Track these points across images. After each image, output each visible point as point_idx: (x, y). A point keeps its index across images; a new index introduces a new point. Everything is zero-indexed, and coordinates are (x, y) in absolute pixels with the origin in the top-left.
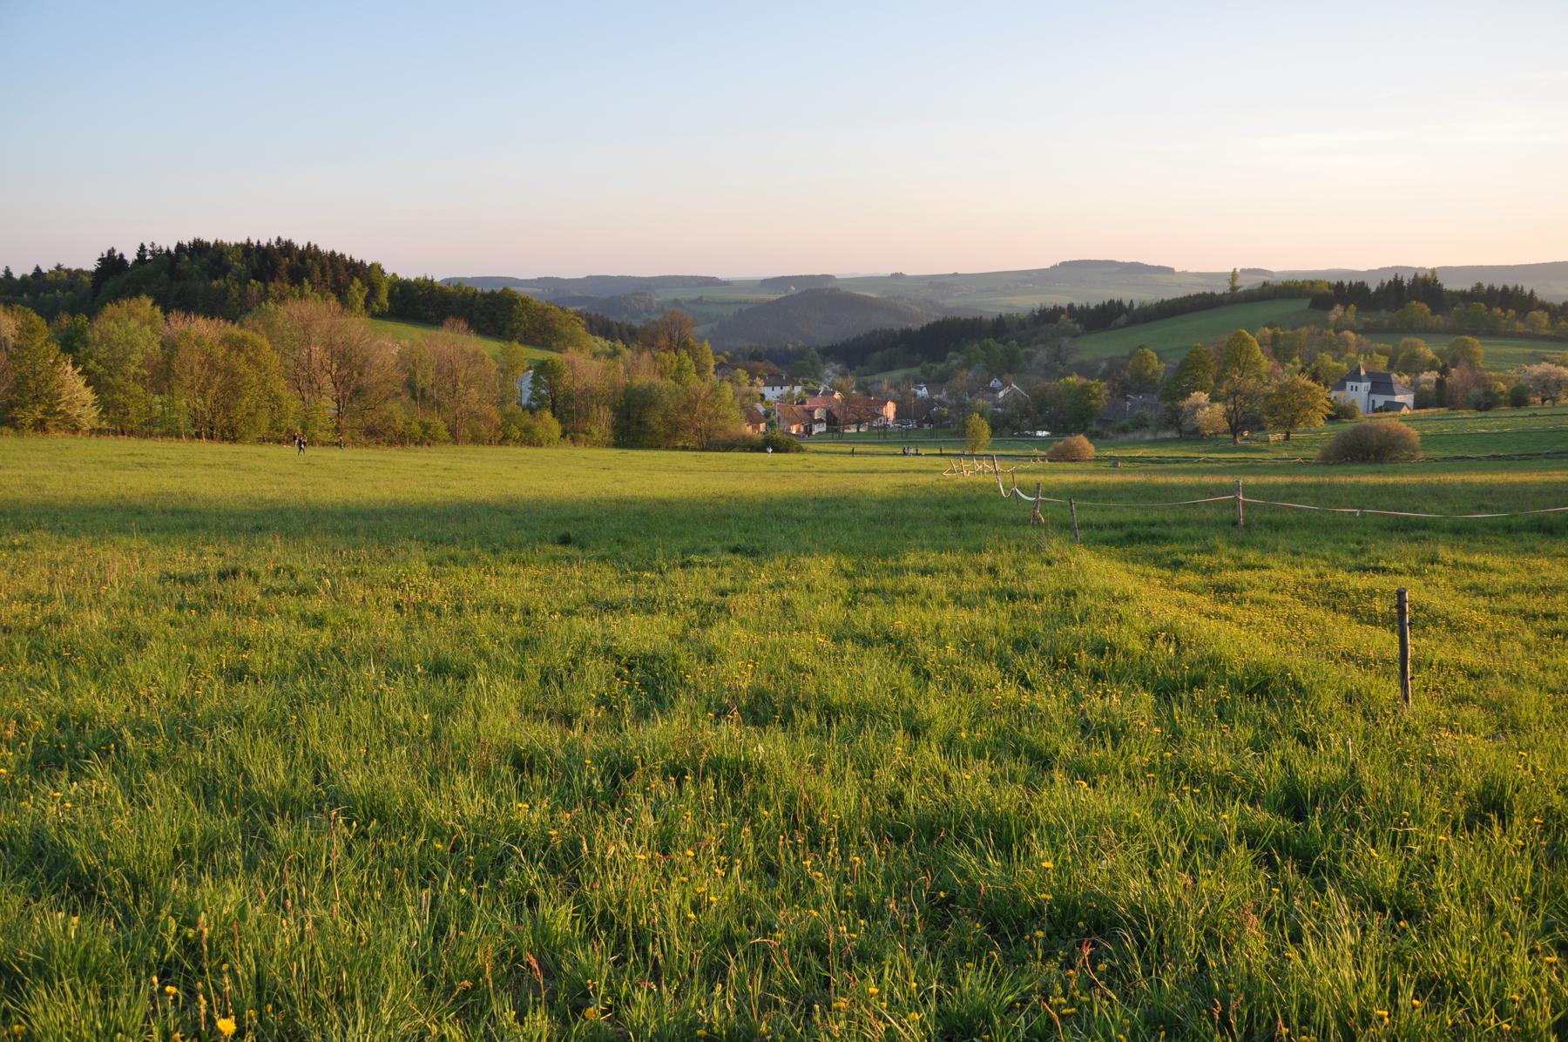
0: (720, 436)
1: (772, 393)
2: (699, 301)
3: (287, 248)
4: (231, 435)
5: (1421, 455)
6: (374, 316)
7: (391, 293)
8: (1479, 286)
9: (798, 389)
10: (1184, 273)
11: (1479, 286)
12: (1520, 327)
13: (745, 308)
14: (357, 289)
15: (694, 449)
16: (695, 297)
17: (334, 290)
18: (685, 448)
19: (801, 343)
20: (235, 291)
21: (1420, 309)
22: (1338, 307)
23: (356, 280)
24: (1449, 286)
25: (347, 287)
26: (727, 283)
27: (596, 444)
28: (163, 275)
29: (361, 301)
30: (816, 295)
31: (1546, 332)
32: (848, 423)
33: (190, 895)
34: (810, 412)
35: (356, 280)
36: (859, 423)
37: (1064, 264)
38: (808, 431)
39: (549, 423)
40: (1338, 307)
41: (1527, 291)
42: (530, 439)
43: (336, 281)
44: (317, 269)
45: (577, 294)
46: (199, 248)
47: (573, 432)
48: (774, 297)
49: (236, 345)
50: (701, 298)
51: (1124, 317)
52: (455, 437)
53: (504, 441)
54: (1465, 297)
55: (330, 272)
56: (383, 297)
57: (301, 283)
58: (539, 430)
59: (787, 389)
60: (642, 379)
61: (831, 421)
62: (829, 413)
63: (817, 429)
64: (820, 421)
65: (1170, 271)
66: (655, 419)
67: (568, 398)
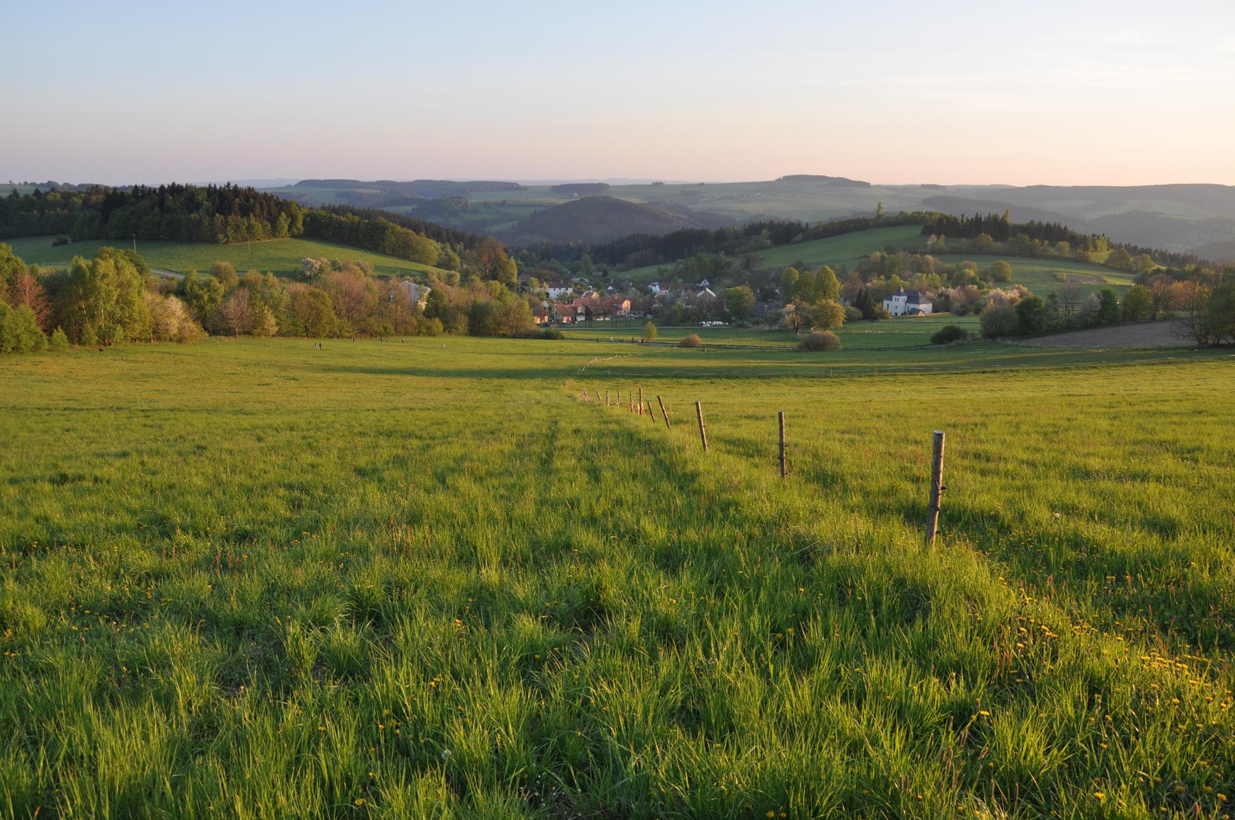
0: (523, 330)
1: (554, 293)
2: (503, 204)
3: (236, 191)
4: (315, 336)
5: (841, 347)
6: (294, 236)
7: (304, 221)
8: (1032, 222)
9: (570, 290)
10: (879, 186)
11: (1032, 222)
12: (1052, 251)
13: (538, 210)
14: (283, 221)
15: (509, 337)
16: (499, 200)
17: (268, 220)
18: (504, 336)
19: (580, 241)
20: (206, 220)
21: (986, 239)
22: (933, 236)
23: (283, 214)
24: (1012, 220)
25: (277, 218)
26: (525, 188)
27: (460, 334)
28: (157, 209)
29: (286, 227)
30: (593, 201)
31: (1067, 255)
32: (598, 315)
33: (37, 682)
34: (575, 309)
35: (283, 214)
36: (605, 315)
37: (786, 178)
38: (574, 319)
39: (438, 324)
40: (933, 236)
41: (1062, 226)
42: (430, 333)
43: (270, 213)
44: (258, 205)
45: (408, 195)
46: (175, 190)
47: (449, 329)
48: (562, 202)
49: (316, 296)
50: (504, 202)
51: (800, 236)
52: (397, 332)
53: (418, 334)
54: (1025, 229)
55: (266, 209)
56: (300, 224)
57: (248, 216)
58: (435, 329)
59: (563, 290)
60: (482, 299)
61: (588, 314)
62: (587, 309)
63: (580, 319)
64: (581, 314)
65: (866, 185)
66: (489, 321)
67: (445, 309)
